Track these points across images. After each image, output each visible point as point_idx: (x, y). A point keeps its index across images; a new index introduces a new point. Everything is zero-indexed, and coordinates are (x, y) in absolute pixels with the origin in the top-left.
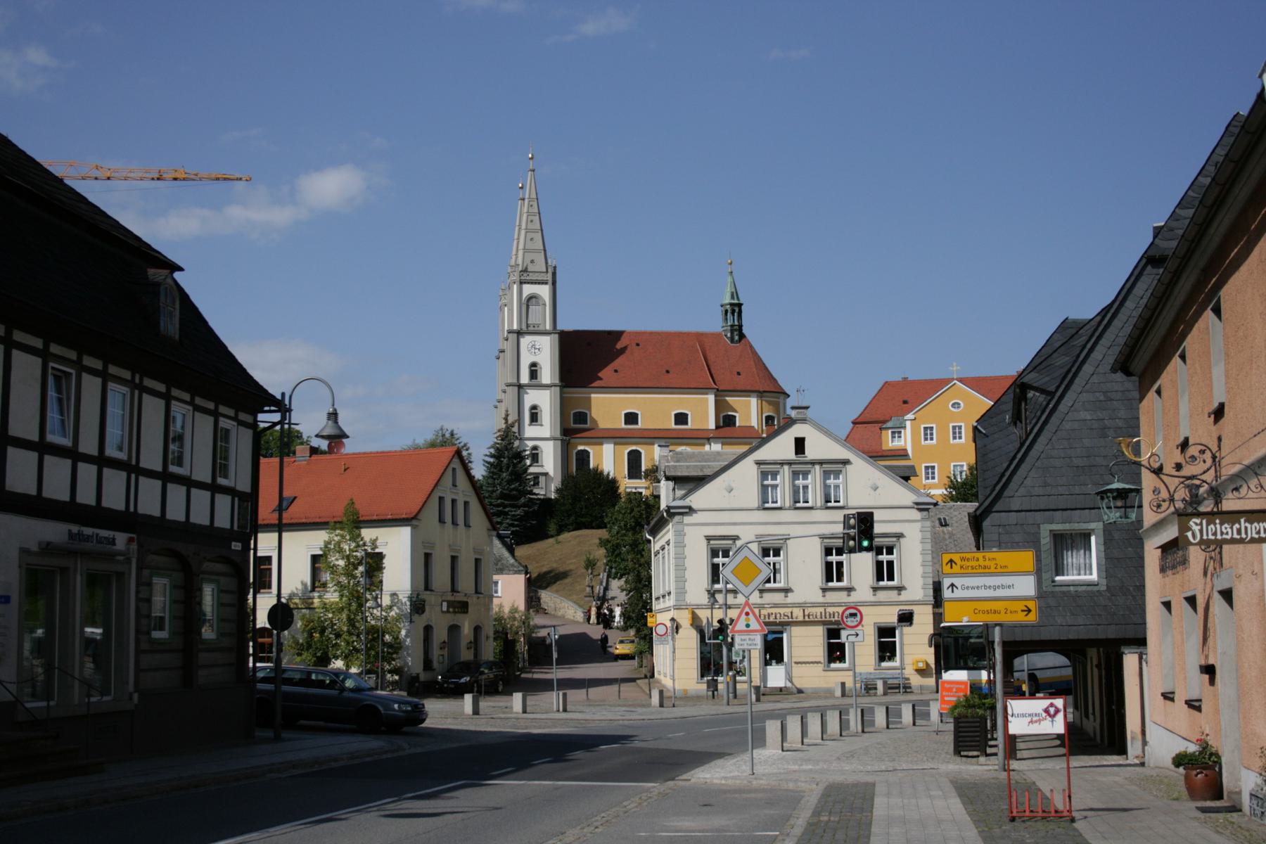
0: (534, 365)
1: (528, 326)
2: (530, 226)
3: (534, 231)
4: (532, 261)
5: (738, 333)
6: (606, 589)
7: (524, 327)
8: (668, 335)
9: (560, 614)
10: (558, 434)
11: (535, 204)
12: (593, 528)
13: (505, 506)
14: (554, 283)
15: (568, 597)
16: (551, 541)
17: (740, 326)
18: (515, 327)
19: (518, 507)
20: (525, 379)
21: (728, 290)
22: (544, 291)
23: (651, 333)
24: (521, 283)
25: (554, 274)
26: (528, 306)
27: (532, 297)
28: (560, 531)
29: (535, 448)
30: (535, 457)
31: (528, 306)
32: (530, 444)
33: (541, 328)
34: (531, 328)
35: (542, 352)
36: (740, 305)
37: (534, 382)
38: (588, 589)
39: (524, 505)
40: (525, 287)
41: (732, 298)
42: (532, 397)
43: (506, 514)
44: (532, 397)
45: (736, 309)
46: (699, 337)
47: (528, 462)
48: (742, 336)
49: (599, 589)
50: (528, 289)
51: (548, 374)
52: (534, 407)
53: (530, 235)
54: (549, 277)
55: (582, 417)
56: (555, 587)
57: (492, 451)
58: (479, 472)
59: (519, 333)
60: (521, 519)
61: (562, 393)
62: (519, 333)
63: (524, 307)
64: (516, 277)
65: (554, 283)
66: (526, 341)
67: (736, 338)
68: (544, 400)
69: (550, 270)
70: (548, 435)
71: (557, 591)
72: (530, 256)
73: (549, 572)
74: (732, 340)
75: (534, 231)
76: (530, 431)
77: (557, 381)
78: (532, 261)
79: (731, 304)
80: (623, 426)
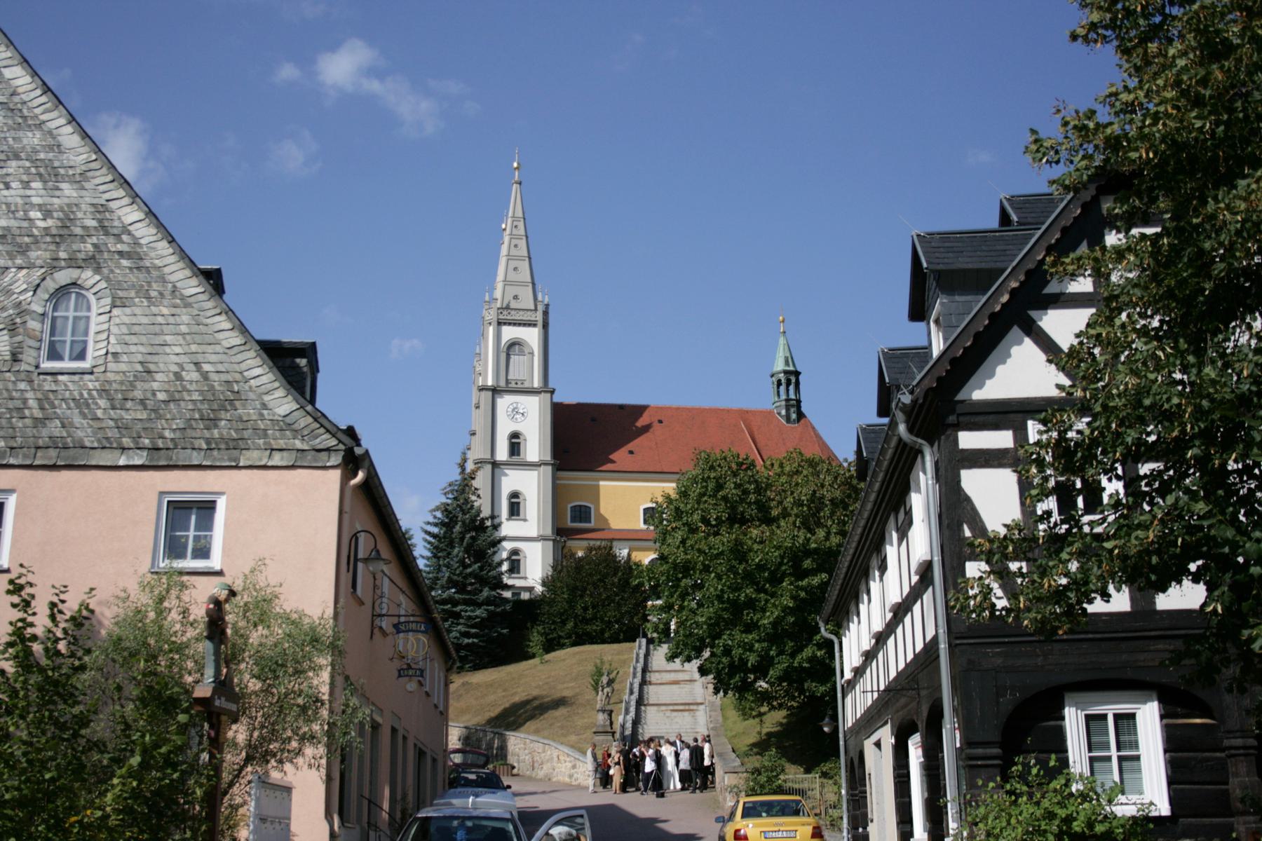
0: (515, 435)
1: (507, 381)
2: (514, 252)
3: (519, 258)
4: (516, 297)
5: (795, 408)
6: (636, 722)
7: (502, 383)
8: (701, 411)
9: (541, 774)
10: (548, 531)
11: (521, 225)
12: (603, 642)
13: (455, 603)
14: (545, 326)
15: (560, 737)
16: (536, 661)
17: (799, 401)
18: (490, 383)
19: (479, 605)
20: (502, 454)
21: (781, 354)
22: (532, 336)
23: (678, 409)
24: (500, 323)
25: (546, 313)
26: (508, 356)
27: (514, 344)
28: (551, 645)
29: (515, 552)
30: (515, 567)
31: (508, 356)
32: (508, 545)
33: (527, 385)
34: (513, 385)
35: (528, 419)
36: (797, 374)
37: (515, 459)
38: (602, 718)
39: (488, 602)
40: (505, 329)
41: (787, 363)
42: (512, 481)
43: (457, 616)
44: (512, 481)
45: (792, 377)
46: (744, 414)
47: (505, 567)
48: (801, 415)
49: (623, 719)
50: (509, 333)
51: (536, 447)
52: (515, 495)
53: (513, 264)
54: (539, 317)
55: (582, 513)
56: (530, 725)
57: (439, 514)
58: (421, 551)
59: (495, 391)
60: (482, 624)
61: (554, 478)
62: (495, 391)
63: (503, 356)
64: (491, 315)
65: (545, 326)
66: (504, 402)
67: (794, 416)
68: (531, 484)
69: (541, 308)
70: (534, 533)
71: (537, 732)
72: (511, 291)
73: (527, 702)
74: (788, 419)
75: (519, 258)
76: (509, 528)
77: (548, 458)
78: (516, 297)
79: (786, 372)
80: (642, 526)
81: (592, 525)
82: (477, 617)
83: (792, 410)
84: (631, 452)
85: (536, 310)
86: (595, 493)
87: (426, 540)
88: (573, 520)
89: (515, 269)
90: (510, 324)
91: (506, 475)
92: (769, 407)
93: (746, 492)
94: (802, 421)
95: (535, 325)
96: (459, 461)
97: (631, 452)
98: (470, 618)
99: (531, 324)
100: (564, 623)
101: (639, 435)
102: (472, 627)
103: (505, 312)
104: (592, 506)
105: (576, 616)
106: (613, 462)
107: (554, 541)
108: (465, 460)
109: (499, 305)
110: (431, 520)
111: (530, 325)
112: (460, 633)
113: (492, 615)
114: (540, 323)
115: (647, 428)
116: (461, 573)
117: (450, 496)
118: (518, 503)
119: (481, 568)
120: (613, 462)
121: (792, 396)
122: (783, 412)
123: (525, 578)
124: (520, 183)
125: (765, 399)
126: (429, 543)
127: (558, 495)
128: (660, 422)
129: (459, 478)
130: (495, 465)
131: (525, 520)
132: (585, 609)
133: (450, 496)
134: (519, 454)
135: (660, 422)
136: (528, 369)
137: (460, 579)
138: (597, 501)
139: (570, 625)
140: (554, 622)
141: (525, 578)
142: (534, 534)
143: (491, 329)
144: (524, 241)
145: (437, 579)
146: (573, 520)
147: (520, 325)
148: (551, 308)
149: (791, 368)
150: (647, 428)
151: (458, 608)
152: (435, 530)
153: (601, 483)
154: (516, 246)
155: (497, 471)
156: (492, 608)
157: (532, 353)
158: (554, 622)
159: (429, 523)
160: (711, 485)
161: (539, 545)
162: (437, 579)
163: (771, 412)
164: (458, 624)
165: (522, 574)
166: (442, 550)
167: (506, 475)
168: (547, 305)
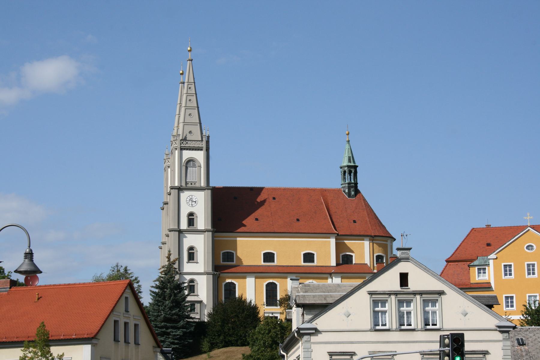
1: (186, 183)
3: (192, 108)
4: (190, 132)
5: (354, 189)
7: (183, 184)
10: (210, 270)
12: (238, 346)
13: (168, 328)
14: (208, 150)
16: (204, 356)
17: (356, 184)
18: (176, 184)
19: (179, 328)
20: (184, 225)
21: (346, 155)
22: (200, 156)
23: (285, 189)
24: (182, 149)
25: (208, 142)
27: (190, 161)
28: (213, 346)
29: (192, 281)
32: (188, 277)
33: (197, 185)
34: (189, 185)
35: (199, 204)
36: (355, 167)
37: (191, 228)
39: (183, 327)
40: (185, 152)
41: (350, 161)
42: (189, 240)
43: (169, 334)
45: (352, 170)
46: (323, 192)
48: (357, 192)
50: (187, 155)
51: (203, 221)
52: (191, 248)
53: (188, 112)
54: (204, 143)
55: (229, 256)
57: (157, 283)
59: (180, 189)
60: (181, 338)
61: (213, 237)
62: (180, 189)
65: (208, 150)
66: (185, 195)
67: (353, 193)
68: (200, 243)
69: (205, 139)
72: (188, 128)
75: (192, 108)
76: (188, 267)
77: (210, 227)
78: (190, 132)
80: (262, 263)
81: (234, 263)
82: (178, 335)
83: (352, 189)
84: (257, 219)
85: (202, 140)
86: (234, 244)
87: (151, 294)
88: (224, 260)
89: (190, 115)
90: (187, 149)
91: (186, 237)
92: (340, 187)
93: (277, 334)
94: (358, 196)
95: (202, 150)
96: (167, 255)
97: (257, 219)
98: (175, 335)
99: (200, 149)
100: (219, 336)
101: (259, 208)
102: (176, 339)
103: (185, 143)
104: (234, 253)
105: (225, 333)
106: (245, 226)
107: (213, 274)
108: (170, 255)
109: (181, 138)
110: (154, 285)
111: (198, 150)
112: (170, 342)
113: (185, 333)
114: (205, 148)
115: (263, 203)
116: (170, 313)
117: (163, 273)
118: (193, 253)
119: (179, 311)
120: (245, 226)
121: (353, 181)
122: (347, 191)
123: (197, 295)
124: (192, 60)
125: (335, 182)
126: (153, 292)
127: (215, 246)
128: (274, 198)
129: (167, 263)
130: (180, 232)
131: (197, 263)
132: (229, 330)
133: (163, 273)
134: (193, 225)
135: (274, 198)
136: (198, 176)
137: (169, 316)
138: (236, 250)
139: (222, 338)
140: (215, 335)
141: (197, 295)
142: (202, 271)
143: (177, 152)
144: (195, 97)
145: (158, 316)
146: (224, 260)
147: (193, 149)
148: (210, 138)
149: (352, 164)
150: (263, 203)
151: (169, 330)
152: (157, 291)
153: (238, 239)
154: (190, 100)
155: (181, 235)
156: (185, 330)
157: (200, 166)
158: (215, 335)
159: (153, 287)
160: (267, 332)
161: (205, 277)
162: (158, 316)
163: (339, 190)
164: (169, 338)
165: (195, 294)
166: (160, 302)
167: (186, 237)
168: (208, 137)
